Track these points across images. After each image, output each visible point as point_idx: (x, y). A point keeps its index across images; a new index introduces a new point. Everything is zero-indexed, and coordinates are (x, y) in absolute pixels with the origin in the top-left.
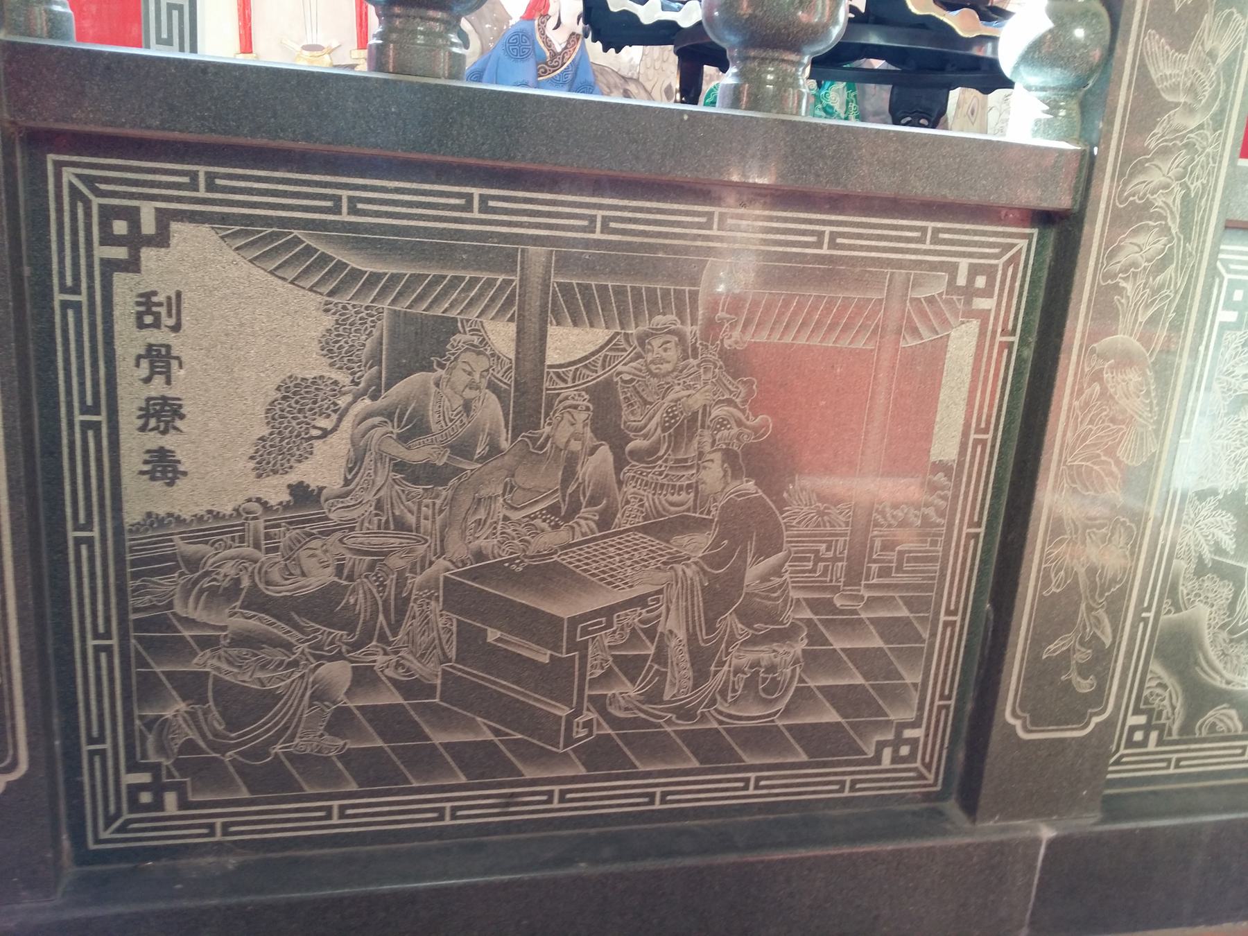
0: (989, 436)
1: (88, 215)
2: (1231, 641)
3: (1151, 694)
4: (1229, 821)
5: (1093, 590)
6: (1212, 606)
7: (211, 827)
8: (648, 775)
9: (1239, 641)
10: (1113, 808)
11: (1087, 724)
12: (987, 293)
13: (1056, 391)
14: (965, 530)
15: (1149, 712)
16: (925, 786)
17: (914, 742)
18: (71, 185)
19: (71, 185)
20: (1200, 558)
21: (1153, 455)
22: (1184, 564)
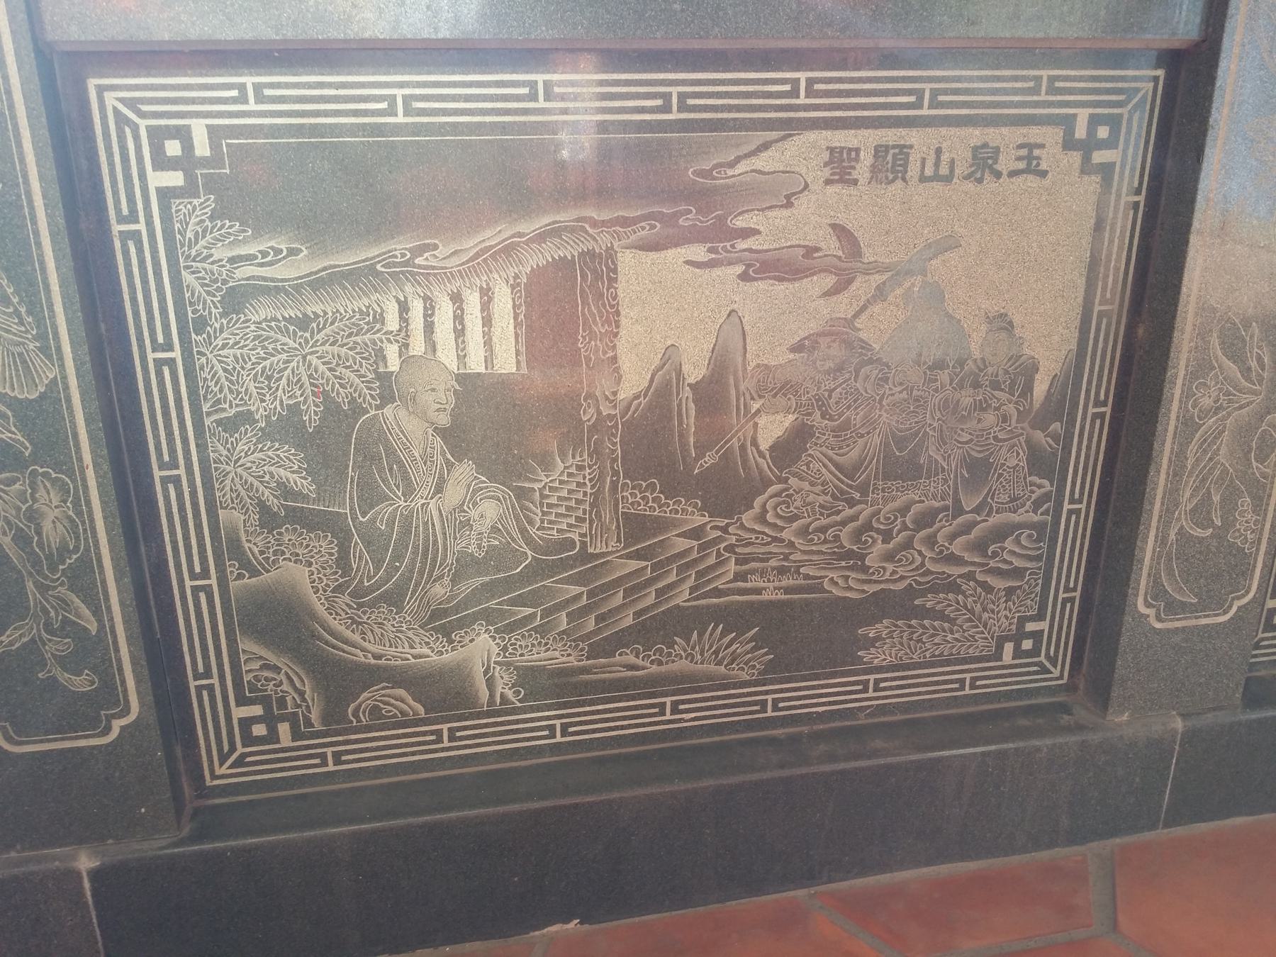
1: (137, 138)
2: (360, 606)
3: (257, 678)
4: (374, 832)
5: (36, 563)
6: (310, 564)
7: (323, 757)
9: (373, 604)
10: (211, 822)
11: (1230, 607)
12: (1110, 144)
14: (1091, 410)
15: (265, 701)
16: (1051, 679)
17: (1037, 635)
18: (115, 108)
20: (263, 507)
21: (54, 380)
22: (238, 517)
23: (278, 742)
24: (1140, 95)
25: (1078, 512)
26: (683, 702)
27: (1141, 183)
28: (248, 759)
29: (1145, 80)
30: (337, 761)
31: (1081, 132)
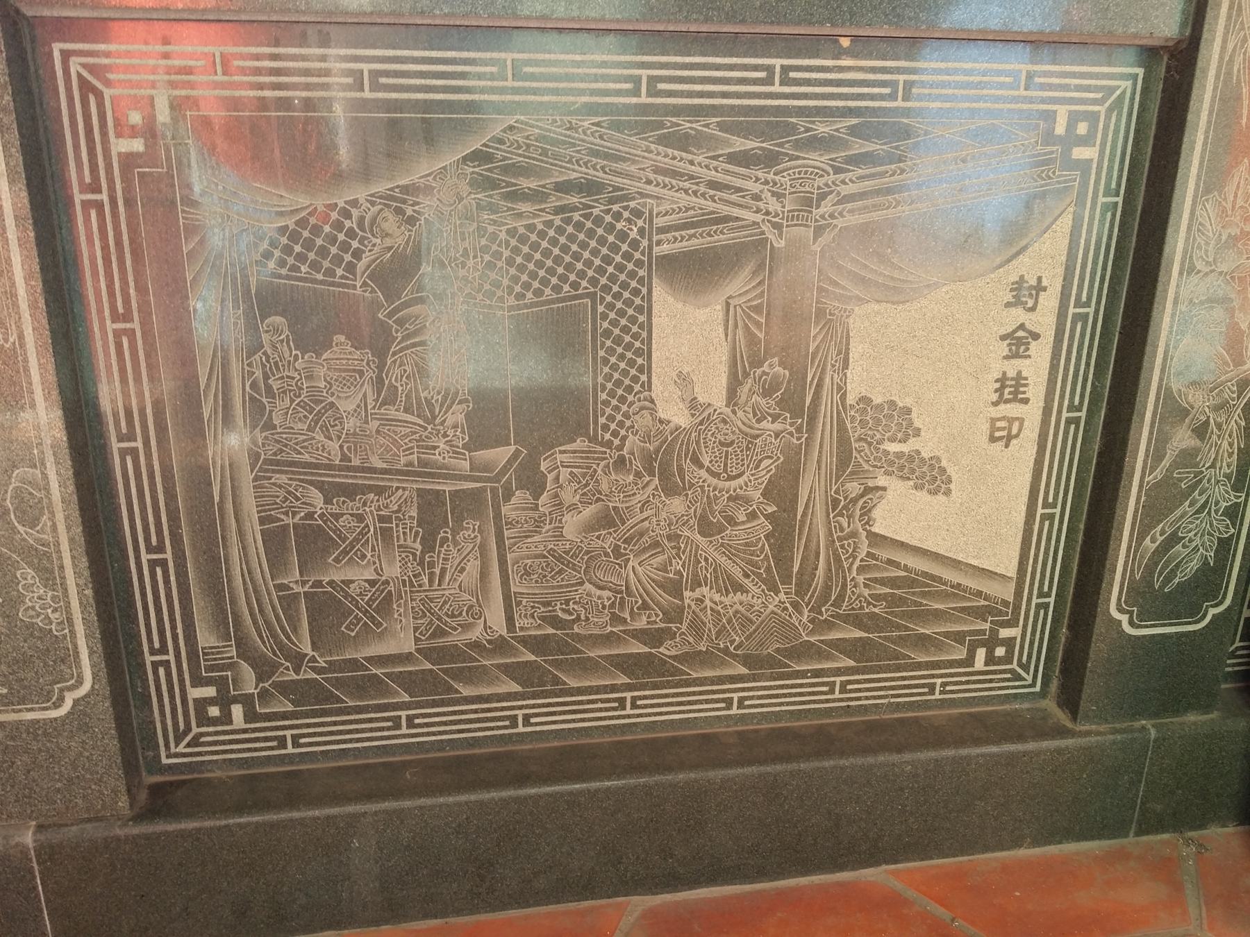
0: (1091, 310)
8: (580, 691)
11: (1204, 616)
12: (1086, 141)
13: (1182, 163)
18: (79, 75)
19: (79, 75)
23: (231, 722)
24: (1118, 92)
25: (1052, 517)
26: (641, 698)
27: (1119, 185)
28: (203, 739)
29: (1122, 78)
30: (296, 744)
31: (1060, 129)
